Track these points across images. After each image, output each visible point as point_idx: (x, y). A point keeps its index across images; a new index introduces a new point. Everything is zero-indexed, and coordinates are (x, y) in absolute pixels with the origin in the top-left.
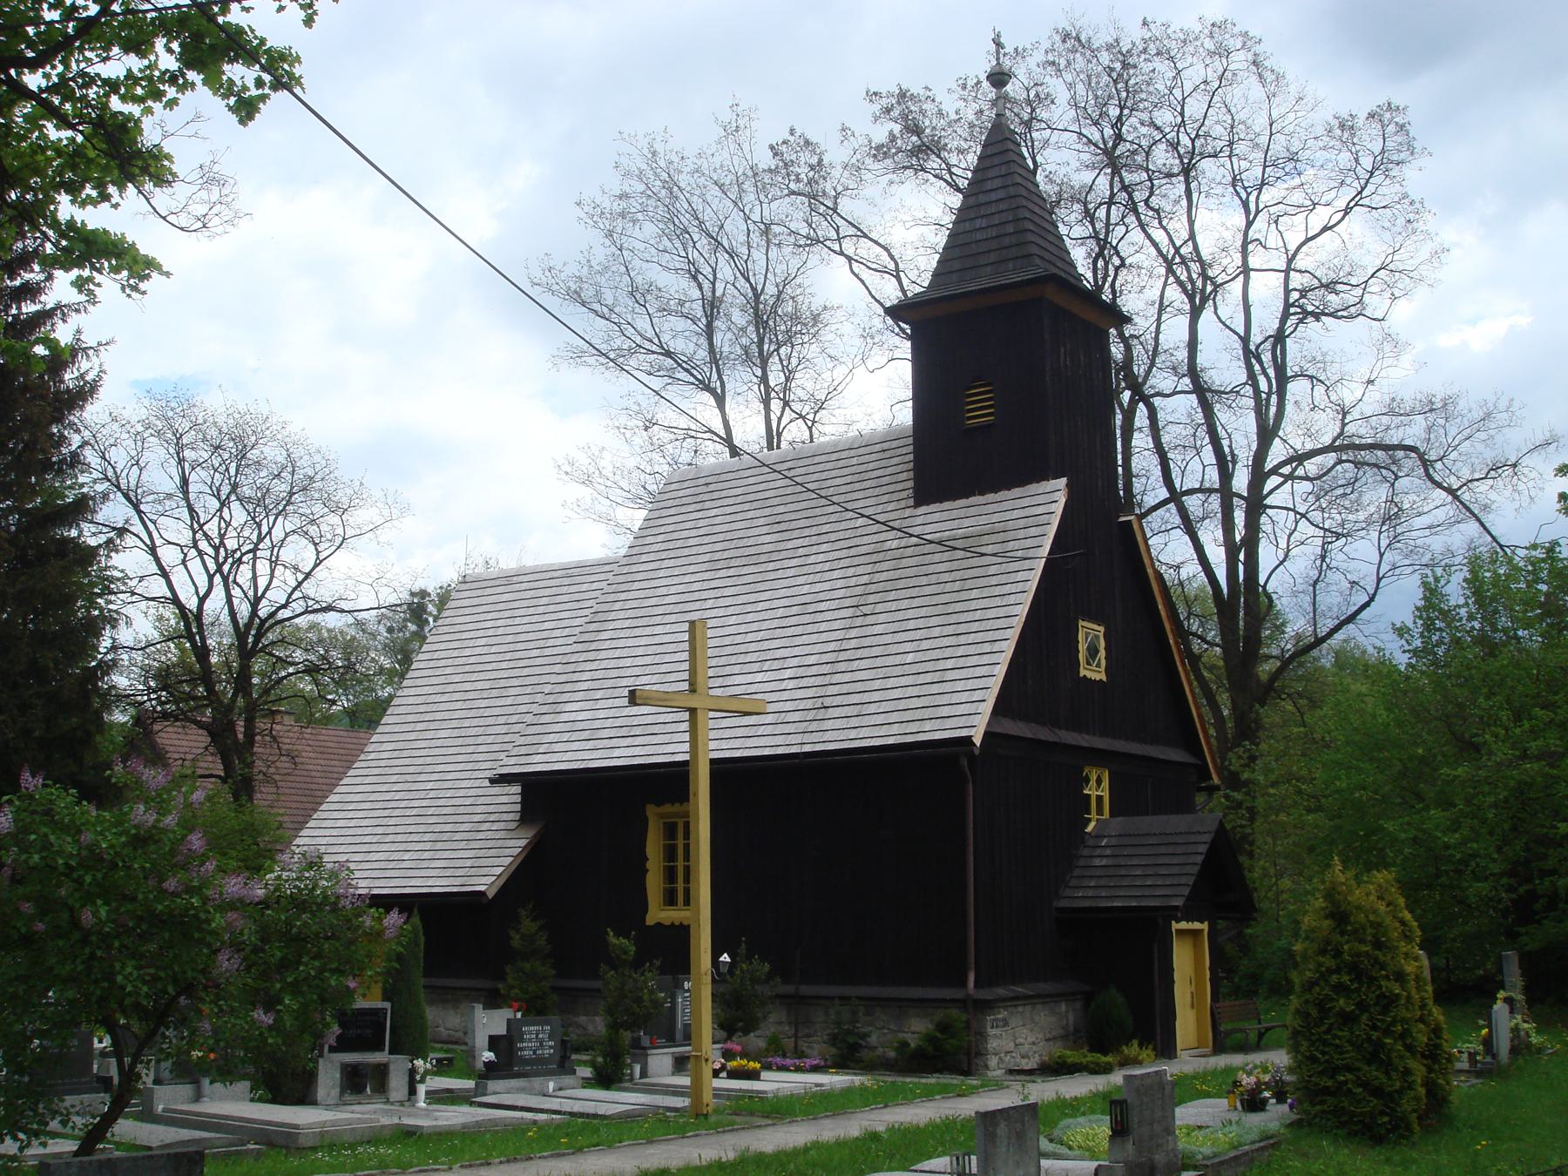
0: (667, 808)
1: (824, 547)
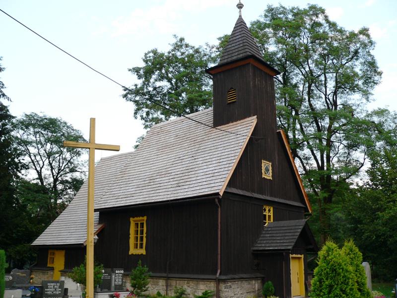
0: (136, 219)
1: (188, 141)
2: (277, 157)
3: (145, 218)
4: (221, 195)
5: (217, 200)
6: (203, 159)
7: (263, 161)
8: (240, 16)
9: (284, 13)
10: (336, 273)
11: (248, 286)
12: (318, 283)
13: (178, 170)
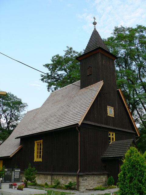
0: (37, 141)
2: (117, 105)
3: (42, 141)
4: (80, 125)
5: (77, 128)
6: (73, 106)
7: (108, 106)
8: (95, 29)
9: (124, 30)
10: (135, 169)
11: (98, 179)
12: (123, 175)
13: (60, 113)
